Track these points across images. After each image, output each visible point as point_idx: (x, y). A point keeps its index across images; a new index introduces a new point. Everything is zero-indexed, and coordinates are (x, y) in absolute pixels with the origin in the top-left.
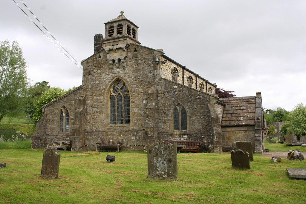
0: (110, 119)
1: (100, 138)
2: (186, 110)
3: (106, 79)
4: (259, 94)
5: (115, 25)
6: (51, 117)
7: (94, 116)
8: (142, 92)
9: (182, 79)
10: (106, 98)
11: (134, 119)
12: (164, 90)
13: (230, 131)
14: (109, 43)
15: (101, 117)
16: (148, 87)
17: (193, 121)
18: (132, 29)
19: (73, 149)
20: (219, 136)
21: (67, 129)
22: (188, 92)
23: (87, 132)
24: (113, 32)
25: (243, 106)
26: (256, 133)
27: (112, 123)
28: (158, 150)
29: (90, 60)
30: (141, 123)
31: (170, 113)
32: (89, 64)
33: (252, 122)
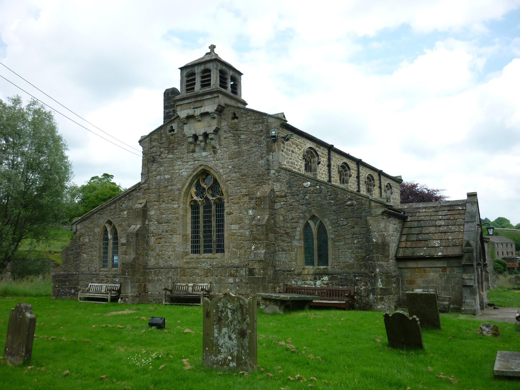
0: (190, 244)
1: (172, 280)
2: (327, 228)
3: (182, 171)
4: (472, 196)
5: (198, 70)
6: (87, 240)
7: (161, 238)
8: (246, 195)
9: (327, 168)
10: (182, 206)
11: (231, 245)
12: (286, 191)
13: (415, 268)
14: (187, 103)
15: (174, 240)
16: (258, 186)
17: (339, 250)
18: (229, 77)
19: (122, 298)
20: (387, 277)
21: (115, 262)
22: (329, 194)
23: (148, 269)
24: (194, 84)
25: (440, 220)
26: (464, 271)
27: (194, 252)
28: (222, 312)
29: (155, 137)
30: (245, 252)
31: (298, 233)
32: (154, 144)
33: (456, 251)
